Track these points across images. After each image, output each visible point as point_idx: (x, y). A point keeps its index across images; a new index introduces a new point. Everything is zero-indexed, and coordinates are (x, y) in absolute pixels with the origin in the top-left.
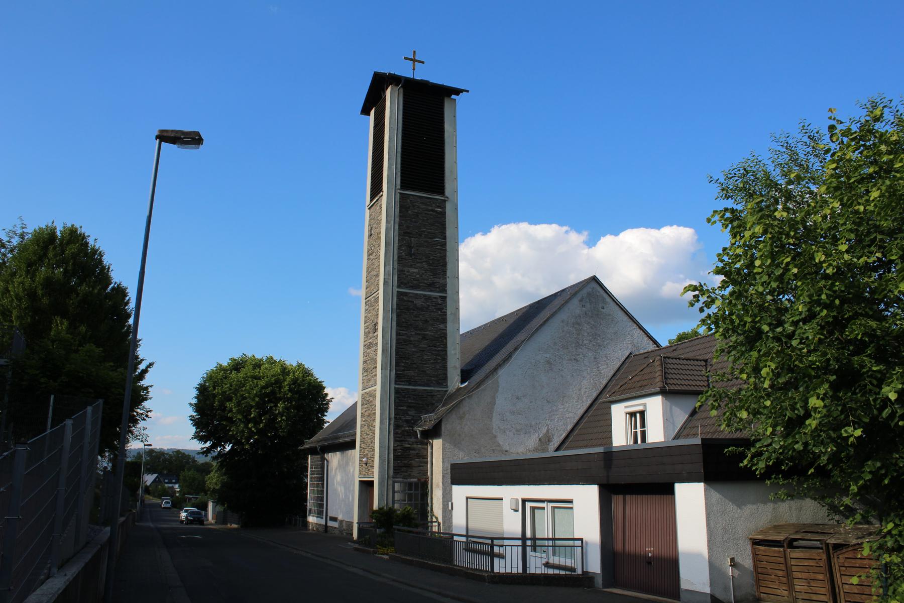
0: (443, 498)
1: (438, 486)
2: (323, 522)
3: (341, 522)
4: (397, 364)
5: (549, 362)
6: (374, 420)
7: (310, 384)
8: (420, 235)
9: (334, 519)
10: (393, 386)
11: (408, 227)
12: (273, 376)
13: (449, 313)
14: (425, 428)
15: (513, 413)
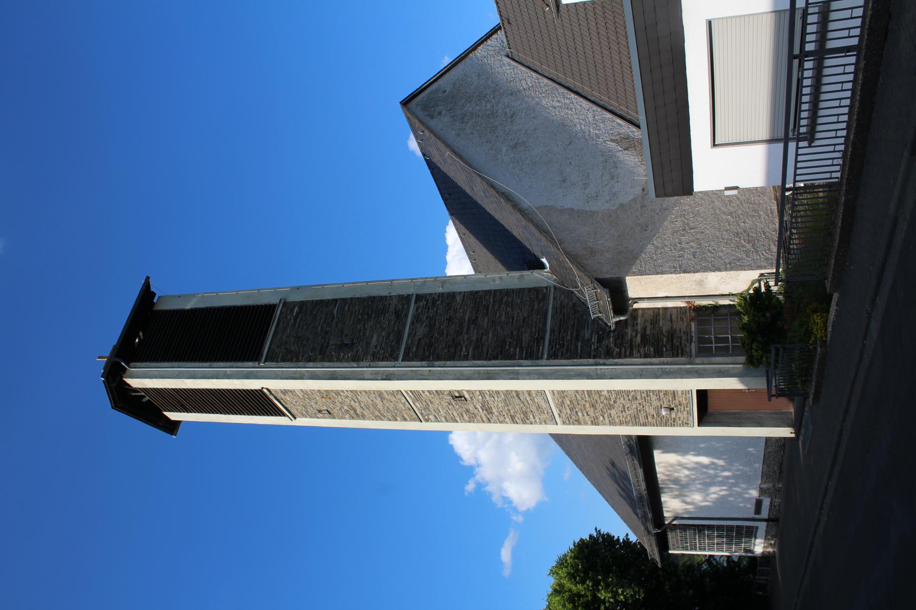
0: (719, 270)
1: (700, 283)
2: (762, 526)
3: (762, 491)
4: (511, 357)
5: (514, 147)
6: (599, 392)
7: (575, 558)
8: (327, 332)
9: (759, 504)
10: (544, 362)
11: (313, 350)
12: (564, 606)
13: (440, 290)
14: (609, 307)
15: (586, 186)
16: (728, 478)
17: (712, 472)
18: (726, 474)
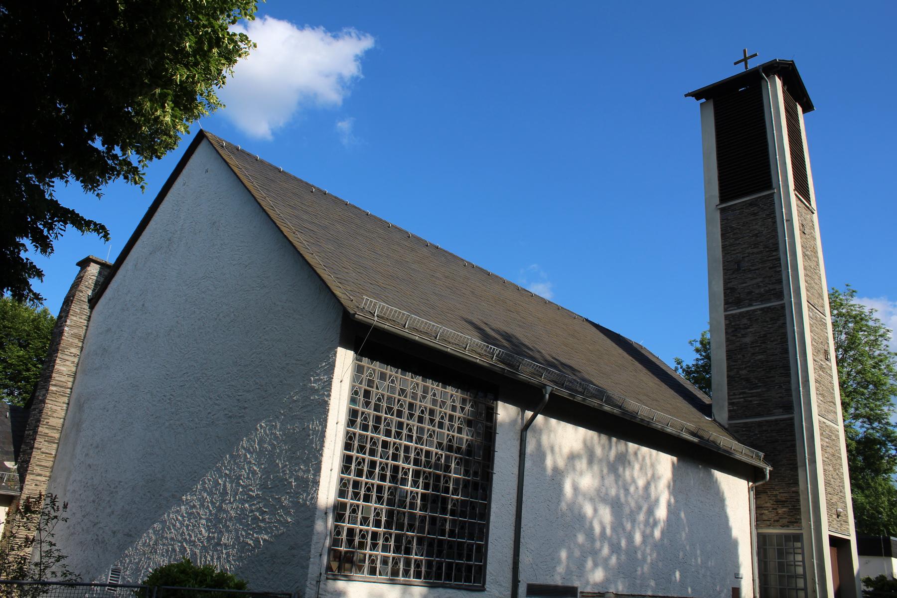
16: (630, 539)
17: (641, 517)
18: (638, 538)
